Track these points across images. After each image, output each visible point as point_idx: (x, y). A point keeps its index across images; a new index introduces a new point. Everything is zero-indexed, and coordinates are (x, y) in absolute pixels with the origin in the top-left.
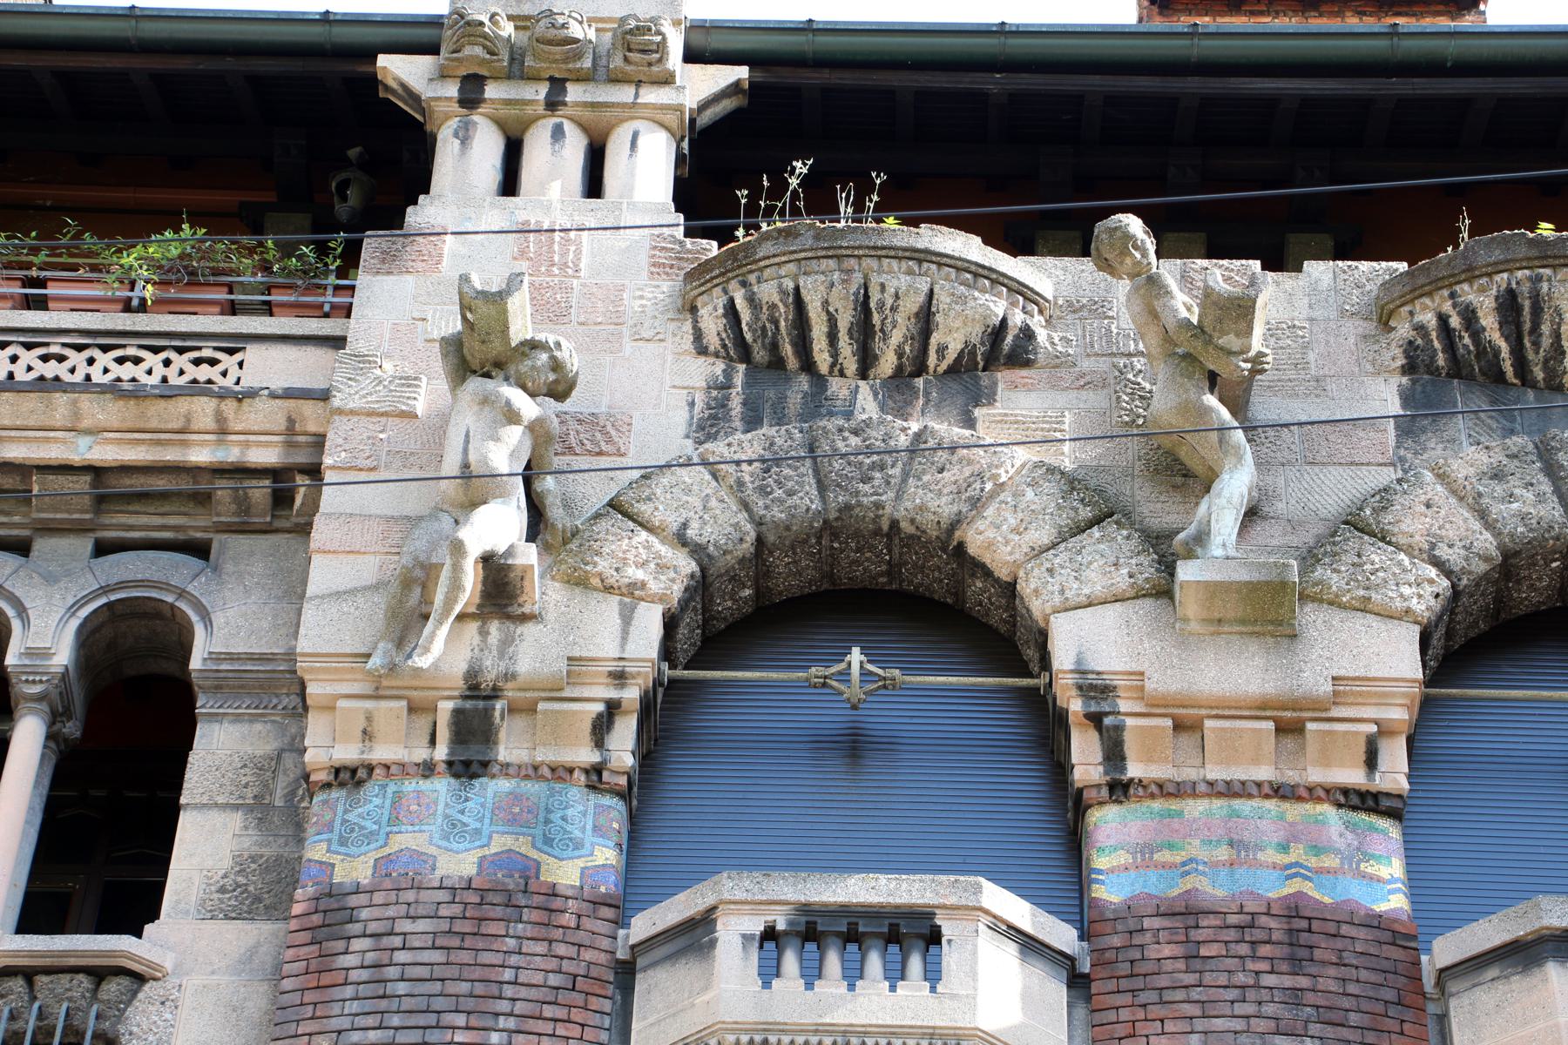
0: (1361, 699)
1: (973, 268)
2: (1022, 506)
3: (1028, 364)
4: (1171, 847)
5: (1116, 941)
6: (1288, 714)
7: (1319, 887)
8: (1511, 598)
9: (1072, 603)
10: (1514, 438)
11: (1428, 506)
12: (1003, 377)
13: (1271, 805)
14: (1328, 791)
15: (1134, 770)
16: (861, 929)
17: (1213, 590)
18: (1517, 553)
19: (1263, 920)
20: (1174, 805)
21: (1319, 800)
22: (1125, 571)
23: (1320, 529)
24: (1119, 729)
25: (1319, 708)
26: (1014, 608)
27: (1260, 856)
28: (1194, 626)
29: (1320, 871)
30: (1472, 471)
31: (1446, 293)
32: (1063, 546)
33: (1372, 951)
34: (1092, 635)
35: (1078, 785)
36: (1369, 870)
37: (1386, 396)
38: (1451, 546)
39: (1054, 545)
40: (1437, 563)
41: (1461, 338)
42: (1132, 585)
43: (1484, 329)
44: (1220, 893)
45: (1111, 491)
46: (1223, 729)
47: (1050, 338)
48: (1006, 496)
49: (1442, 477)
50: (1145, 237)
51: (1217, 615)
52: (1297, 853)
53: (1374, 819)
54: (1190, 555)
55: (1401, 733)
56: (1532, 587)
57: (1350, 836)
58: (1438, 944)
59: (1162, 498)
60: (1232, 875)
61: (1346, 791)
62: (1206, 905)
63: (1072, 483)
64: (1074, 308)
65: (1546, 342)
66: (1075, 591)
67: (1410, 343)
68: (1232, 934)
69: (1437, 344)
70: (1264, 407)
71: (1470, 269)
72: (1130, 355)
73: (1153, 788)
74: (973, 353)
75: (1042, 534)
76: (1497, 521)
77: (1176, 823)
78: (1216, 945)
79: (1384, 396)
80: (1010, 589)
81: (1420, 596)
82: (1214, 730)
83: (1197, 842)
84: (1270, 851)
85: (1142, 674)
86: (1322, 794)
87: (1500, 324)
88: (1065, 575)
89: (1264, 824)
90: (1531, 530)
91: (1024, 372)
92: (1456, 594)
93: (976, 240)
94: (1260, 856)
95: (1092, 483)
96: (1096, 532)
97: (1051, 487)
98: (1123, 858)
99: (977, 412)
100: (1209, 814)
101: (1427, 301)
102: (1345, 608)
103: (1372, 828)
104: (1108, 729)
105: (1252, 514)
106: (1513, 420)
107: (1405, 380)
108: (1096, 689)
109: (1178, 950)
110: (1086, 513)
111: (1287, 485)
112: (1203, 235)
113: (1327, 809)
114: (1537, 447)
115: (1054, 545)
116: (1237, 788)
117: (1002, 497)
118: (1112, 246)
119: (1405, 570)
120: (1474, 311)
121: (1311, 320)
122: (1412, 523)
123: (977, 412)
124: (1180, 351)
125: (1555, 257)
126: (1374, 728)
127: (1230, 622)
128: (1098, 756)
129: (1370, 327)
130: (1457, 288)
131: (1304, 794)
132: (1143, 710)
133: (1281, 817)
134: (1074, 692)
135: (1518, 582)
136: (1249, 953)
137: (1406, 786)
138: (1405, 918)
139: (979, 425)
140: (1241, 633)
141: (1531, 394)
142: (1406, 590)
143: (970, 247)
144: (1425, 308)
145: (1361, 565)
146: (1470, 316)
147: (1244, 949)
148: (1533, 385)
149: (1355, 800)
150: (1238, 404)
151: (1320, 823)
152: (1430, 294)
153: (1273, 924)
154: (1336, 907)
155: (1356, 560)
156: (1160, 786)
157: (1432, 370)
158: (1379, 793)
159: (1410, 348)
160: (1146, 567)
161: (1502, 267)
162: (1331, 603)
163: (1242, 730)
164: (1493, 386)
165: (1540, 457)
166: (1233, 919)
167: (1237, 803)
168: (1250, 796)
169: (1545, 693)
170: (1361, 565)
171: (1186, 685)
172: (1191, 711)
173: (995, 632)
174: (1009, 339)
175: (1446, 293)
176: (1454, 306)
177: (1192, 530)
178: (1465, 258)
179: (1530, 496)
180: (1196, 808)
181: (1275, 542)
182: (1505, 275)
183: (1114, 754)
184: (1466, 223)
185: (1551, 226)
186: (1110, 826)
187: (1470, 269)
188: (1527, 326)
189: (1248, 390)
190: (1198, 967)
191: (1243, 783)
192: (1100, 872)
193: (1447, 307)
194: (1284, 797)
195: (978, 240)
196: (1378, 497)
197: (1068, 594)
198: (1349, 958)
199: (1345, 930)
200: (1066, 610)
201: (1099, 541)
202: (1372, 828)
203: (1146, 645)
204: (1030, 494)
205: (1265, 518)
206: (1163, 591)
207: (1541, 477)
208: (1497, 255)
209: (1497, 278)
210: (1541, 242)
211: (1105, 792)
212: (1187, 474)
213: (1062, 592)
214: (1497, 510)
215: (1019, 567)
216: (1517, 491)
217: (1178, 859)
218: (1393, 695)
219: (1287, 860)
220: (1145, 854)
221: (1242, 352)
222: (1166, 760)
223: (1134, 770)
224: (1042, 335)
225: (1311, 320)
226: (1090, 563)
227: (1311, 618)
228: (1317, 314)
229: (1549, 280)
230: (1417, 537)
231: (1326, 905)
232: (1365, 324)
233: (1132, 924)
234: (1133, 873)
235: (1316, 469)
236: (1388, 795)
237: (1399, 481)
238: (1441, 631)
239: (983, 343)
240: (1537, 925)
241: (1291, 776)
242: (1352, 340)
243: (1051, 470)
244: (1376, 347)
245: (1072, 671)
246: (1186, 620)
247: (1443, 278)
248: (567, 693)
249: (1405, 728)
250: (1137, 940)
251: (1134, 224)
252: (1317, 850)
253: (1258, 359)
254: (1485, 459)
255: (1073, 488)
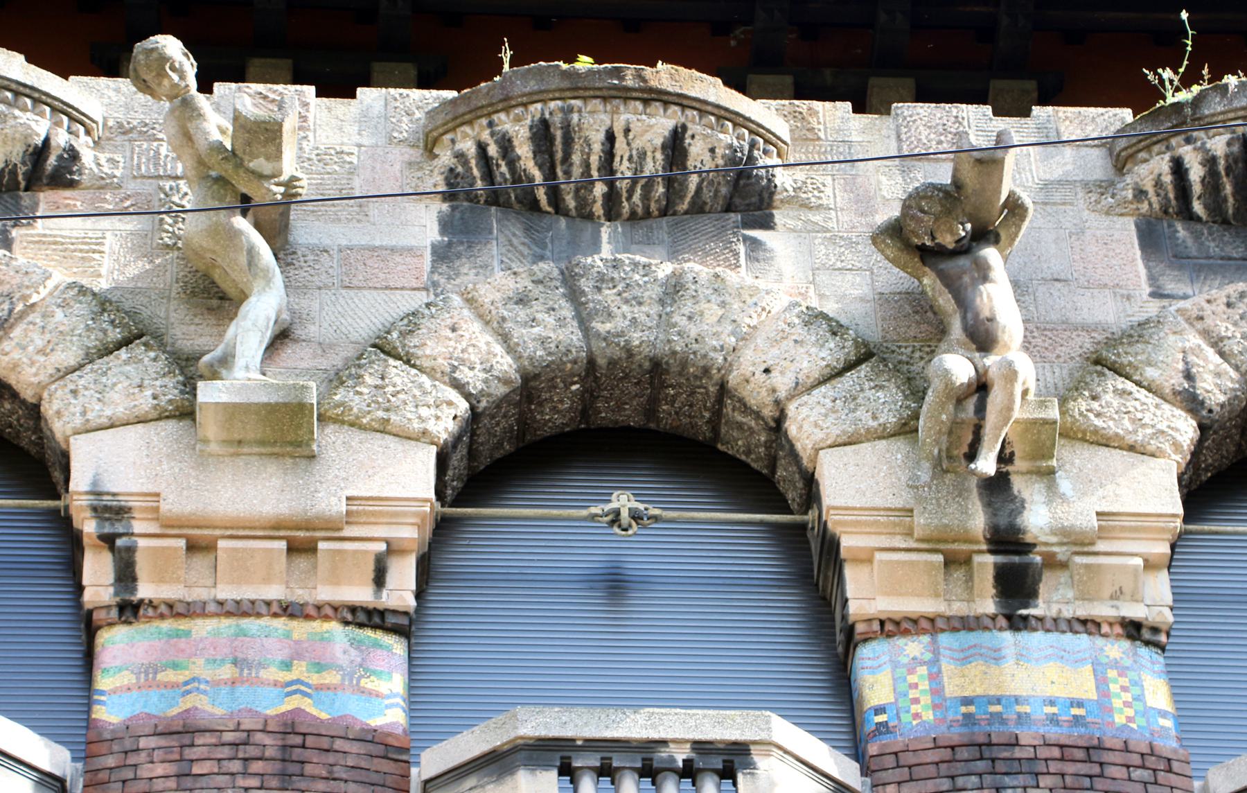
0: (373, 518)
1: (14, 86)
2: (50, 327)
3: (72, 185)
4: (175, 666)
5: (111, 761)
6: (301, 534)
7: (318, 703)
8: (535, 421)
9: (93, 425)
10: (541, 264)
11: (454, 330)
12: (46, 199)
13: (280, 623)
14: (336, 609)
15: (145, 591)
16: (615, 764)
17: (232, 412)
18: (536, 376)
19: (259, 737)
20: (183, 625)
21: (326, 618)
22: (148, 393)
23: (351, 352)
24: (131, 550)
25: (332, 527)
26: (41, 430)
27: (263, 674)
28: (214, 447)
29: (319, 688)
30: (498, 296)
31: (484, 121)
32: (89, 366)
33: (363, 764)
34: (112, 455)
35: (88, 606)
36: (370, 686)
37: (424, 224)
38: (472, 369)
39: (80, 367)
40: (458, 386)
41: (498, 166)
42: (155, 407)
43: (519, 158)
44: (219, 711)
45: (146, 313)
46: (235, 550)
47: (96, 158)
48: (35, 317)
49: (470, 301)
50: (184, 59)
51: (237, 437)
52: (300, 670)
53: (379, 636)
54: (215, 376)
55: (411, 552)
56: (554, 410)
57: (353, 652)
58: (426, 756)
59: (197, 320)
60: (232, 693)
61: (353, 609)
62: (203, 724)
63: (103, 303)
64: (124, 130)
65: (577, 171)
66: (100, 412)
67: (451, 170)
68: (226, 752)
69: (476, 172)
70: (306, 229)
71: (507, 99)
72: (177, 178)
73: (163, 609)
74: (14, 173)
75: (68, 355)
76: (518, 344)
77: (182, 643)
78: (208, 763)
79: (423, 222)
80: (34, 411)
81: (438, 418)
82: (226, 550)
83: (202, 661)
84: (273, 669)
85: (158, 495)
86: (329, 611)
87: (535, 153)
88: (88, 397)
89: (268, 643)
90: (550, 354)
91: (68, 193)
92: (475, 415)
93: (19, 58)
94: (263, 674)
95: (127, 306)
96: (123, 354)
97: (82, 309)
98: (127, 678)
99: (14, 233)
100: (217, 633)
101: (467, 129)
102: (365, 429)
103: (377, 645)
104: (120, 550)
105: (282, 337)
106: (544, 247)
107: (445, 207)
108: (112, 511)
109: (171, 769)
110: (115, 334)
111: (321, 309)
112: (290, 61)
113: (334, 627)
114: (562, 273)
115: (80, 367)
116: (180, 608)
117: (30, 318)
118: (148, 66)
119: (425, 393)
120: (510, 141)
121: (359, 146)
122: (434, 346)
123: (14, 233)
124: (213, 173)
125: (586, 89)
126: (382, 547)
127: (250, 443)
128: (110, 577)
129: (416, 154)
130: (495, 117)
131: (313, 612)
132: (158, 531)
133: (288, 635)
134: (89, 514)
135: (541, 404)
136: (1034, 783)
137: (1171, 619)
138: (399, 731)
139: (15, 246)
140: (261, 454)
141: (563, 222)
142: (424, 412)
143: (711, 89)
144: (465, 135)
145: (383, 387)
146: (506, 145)
147: (236, 766)
148: (566, 214)
149: (362, 617)
150: (276, 231)
151: (325, 640)
152: (470, 123)
153: (268, 740)
154: (333, 721)
155: (379, 382)
156: (170, 606)
157: (471, 197)
158: (386, 610)
159: (451, 175)
160: (170, 390)
161: (535, 98)
162: (352, 425)
163: (253, 550)
164: (528, 214)
165: (565, 282)
166: (229, 737)
167: (246, 623)
168: (259, 615)
169: (555, 512)
170: (383, 387)
171: (201, 506)
172: (206, 532)
173: (26, 453)
174: (52, 161)
175: (484, 121)
176: (492, 134)
177: (218, 352)
178: (503, 88)
179: (550, 320)
180: (202, 628)
181: (304, 365)
182: (539, 106)
183: (126, 575)
184: (506, 55)
185: (591, 60)
186: (118, 645)
187: (507, 99)
188: (559, 155)
189: (285, 215)
190: (189, 785)
191: (253, 602)
192: (102, 693)
193: (485, 136)
194: (292, 616)
195: (21, 58)
196: (406, 321)
197: (90, 416)
198: (340, 772)
199: (339, 745)
200: (88, 431)
201: (126, 363)
202: (377, 645)
203: (165, 467)
204: (59, 314)
205: (296, 341)
206: (186, 412)
207: (563, 302)
208: (532, 86)
209: (532, 108)
210: (573, 75)
211: (114, 613)
212: (223, 297)
213: (84, 413)
214: (519, 334)
215: (44, 387)
216: (539, 316)
217: (181, 679)
218: (405, 514)
219: (289, 676)
220: (149, 675)
221: (274, 176)
222: (178, 580)
223: (145, 591)
224: (87, 157)
225: (359, 146)
226: (115, 385)
227: (329, 440)
228: (365, 141)
229: (580, 111)
230: (440, 361)
231: (322, 721)
232: (412, 151)
233: (128, 744)
234: (135, 693)
235: (352, 293)
236: (395, 612)
237: (428, 305)
238: (462, 450)
239: (24, 163)
240: (513, 735)
241: (300, 595)
242: (397, 167)
243: (83, 291)
244: (419, 174)
245: (87, 493)
246: (206, 441)
247: (482, 107)
248: (348, 532)
249: (415, 547)
250: (132, 760)
251: (171, 45)
252: (320, 667)
253: (290, 183)
254: (512, 285)
255: (104, 310)
